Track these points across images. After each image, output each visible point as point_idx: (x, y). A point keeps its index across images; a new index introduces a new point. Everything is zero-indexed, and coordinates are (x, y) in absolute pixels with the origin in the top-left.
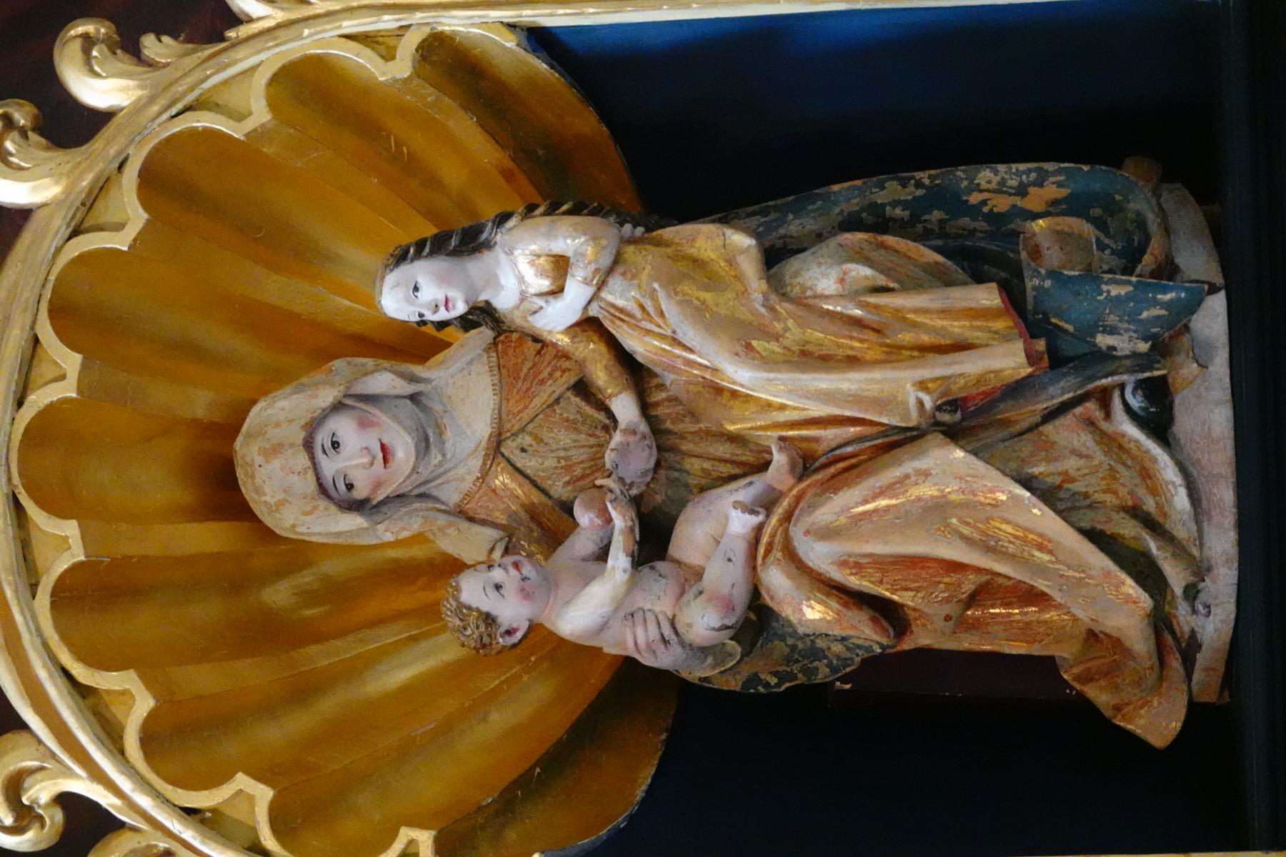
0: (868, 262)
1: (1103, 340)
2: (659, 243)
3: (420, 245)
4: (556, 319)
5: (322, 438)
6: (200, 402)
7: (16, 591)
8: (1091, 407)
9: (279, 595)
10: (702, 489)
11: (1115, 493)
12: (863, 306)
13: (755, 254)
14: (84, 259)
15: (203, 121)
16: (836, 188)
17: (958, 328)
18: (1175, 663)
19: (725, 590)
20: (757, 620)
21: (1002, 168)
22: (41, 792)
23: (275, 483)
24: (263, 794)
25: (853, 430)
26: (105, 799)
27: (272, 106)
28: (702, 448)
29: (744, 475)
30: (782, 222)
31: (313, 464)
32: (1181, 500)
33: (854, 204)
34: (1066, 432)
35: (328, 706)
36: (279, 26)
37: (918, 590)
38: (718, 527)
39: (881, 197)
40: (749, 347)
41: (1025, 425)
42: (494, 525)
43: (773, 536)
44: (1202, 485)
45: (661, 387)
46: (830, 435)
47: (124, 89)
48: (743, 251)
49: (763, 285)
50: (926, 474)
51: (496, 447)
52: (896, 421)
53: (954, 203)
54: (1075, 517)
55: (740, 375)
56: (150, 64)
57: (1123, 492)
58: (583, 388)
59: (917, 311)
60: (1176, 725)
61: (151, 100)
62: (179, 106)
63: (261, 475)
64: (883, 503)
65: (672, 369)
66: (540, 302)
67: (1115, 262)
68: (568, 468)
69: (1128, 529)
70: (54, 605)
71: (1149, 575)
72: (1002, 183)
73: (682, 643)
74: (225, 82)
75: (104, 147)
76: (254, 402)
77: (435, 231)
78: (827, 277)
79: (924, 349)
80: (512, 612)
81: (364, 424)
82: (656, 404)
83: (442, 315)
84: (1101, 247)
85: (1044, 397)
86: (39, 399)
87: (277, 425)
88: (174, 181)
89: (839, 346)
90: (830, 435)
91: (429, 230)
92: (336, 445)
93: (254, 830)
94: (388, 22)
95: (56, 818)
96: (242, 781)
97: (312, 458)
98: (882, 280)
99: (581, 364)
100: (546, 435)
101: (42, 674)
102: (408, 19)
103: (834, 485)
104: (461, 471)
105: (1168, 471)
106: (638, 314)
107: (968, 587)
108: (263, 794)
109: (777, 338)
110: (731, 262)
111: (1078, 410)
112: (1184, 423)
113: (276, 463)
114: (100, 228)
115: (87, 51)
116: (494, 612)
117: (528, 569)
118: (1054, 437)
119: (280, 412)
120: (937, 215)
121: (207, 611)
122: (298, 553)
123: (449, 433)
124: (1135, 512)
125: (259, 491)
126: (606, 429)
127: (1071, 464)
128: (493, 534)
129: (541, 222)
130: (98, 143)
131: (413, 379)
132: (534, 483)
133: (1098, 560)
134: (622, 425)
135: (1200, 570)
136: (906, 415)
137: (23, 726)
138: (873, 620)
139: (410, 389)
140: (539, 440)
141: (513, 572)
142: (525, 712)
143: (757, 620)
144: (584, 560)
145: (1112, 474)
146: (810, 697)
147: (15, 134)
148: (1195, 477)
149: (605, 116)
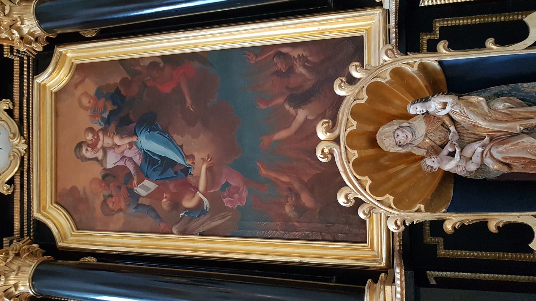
2: (463, 99)
4: (443, 113)
5: (396, 135)
6: (371, 128)
10: (468, 144)
13: (485, 101)
14: (357, 104)
17: (528, 115)
20: (482, 166)
21: (529, 83)
22: (351, 197)
24: (392, 198)
25: (503, 133)
26: (363, 198)
27: (391, 77)
29: (475, 141)
33: (496, 91)
36: (392, 62)
46: (498, 134)
47: (363, 75)
50: (524, 142)
51: (426, 136)
53: (519, 90)
58: (443, 125)
61: (368, 76)
64: (513, 147)
70: (353, 165)
72: (529, 86)
76: (379, 128)
78: (500, 105)
79: (520, 118)
80: (436, 166)
81: (403, 132)
86: (349, 130)
90: (498, 134)
96: (388, 195)
98: (512, 106)
100: (435, 133)
108: (392, 198)
109: (490, 117)
117: (438, 158)
120: (514, 92)
123: (416, 133)
130: (358, 84)
136: (517, 131)
137: (347, 185)
139: (409, 125)
143: (482, 166)
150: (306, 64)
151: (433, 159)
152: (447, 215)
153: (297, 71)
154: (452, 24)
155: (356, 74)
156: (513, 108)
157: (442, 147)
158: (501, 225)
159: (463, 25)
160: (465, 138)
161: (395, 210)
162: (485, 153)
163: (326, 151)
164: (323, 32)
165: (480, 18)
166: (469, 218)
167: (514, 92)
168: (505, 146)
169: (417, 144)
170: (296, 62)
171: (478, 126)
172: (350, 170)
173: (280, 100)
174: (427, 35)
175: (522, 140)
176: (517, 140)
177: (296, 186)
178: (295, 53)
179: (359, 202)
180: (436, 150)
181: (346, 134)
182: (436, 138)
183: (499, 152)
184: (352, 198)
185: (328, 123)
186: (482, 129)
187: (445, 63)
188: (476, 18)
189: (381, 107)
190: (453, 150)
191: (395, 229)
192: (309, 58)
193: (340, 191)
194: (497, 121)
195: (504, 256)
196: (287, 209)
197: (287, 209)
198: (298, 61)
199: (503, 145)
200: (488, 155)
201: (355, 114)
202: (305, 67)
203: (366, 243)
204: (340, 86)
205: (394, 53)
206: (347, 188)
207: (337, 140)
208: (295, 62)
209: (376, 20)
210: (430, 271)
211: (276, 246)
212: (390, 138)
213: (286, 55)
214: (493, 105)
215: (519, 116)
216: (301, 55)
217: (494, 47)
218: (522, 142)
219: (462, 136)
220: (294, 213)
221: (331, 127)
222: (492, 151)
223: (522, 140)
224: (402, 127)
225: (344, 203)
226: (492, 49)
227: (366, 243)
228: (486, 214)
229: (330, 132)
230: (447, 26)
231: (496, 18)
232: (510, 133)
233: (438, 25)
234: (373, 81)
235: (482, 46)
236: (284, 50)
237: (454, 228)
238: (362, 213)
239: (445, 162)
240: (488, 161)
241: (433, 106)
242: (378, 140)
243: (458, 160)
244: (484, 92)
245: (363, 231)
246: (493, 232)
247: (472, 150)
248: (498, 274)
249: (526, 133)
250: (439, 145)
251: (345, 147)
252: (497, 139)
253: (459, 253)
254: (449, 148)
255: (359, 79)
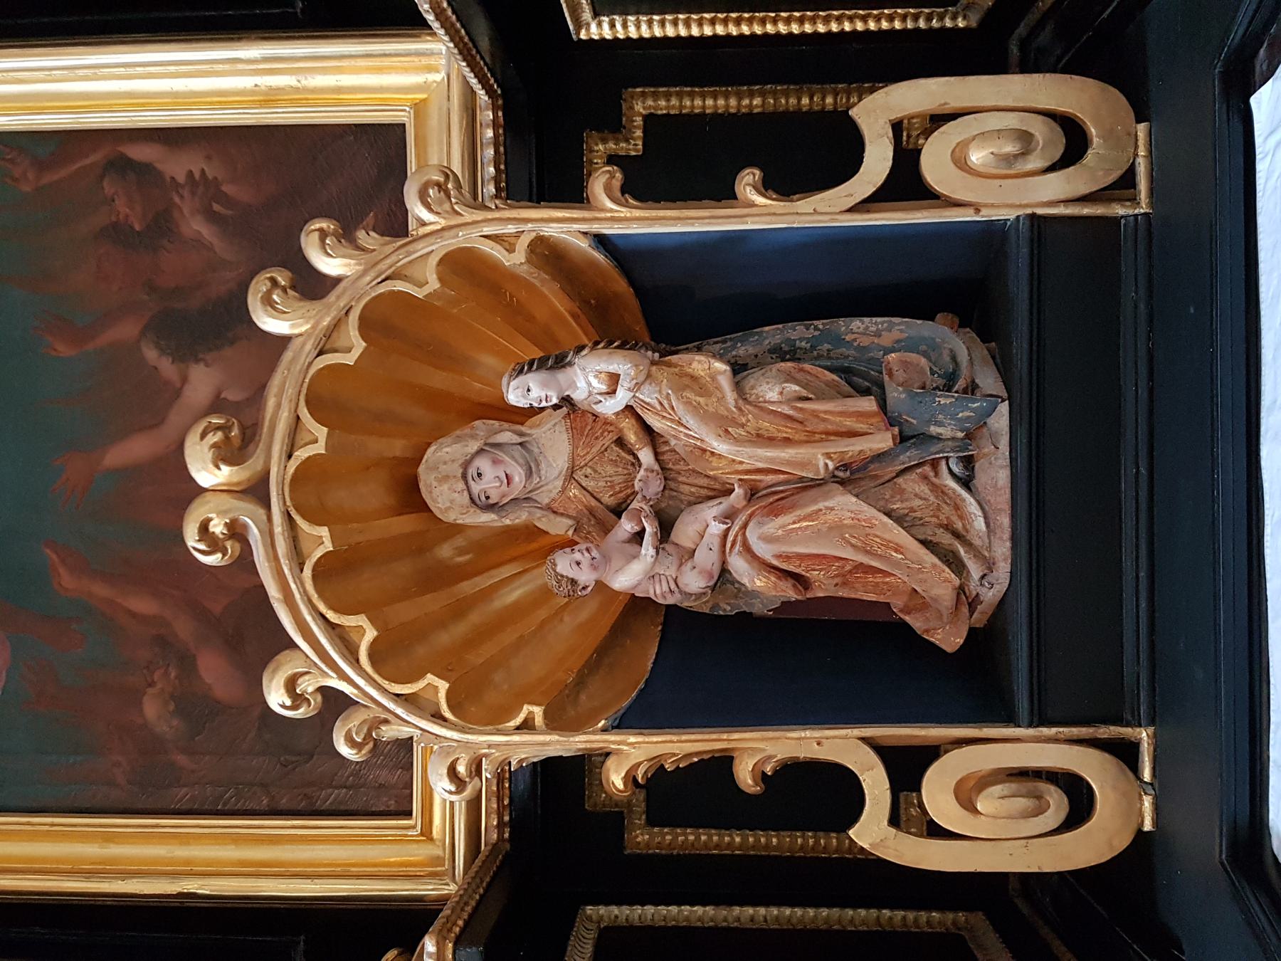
0: (797, 382)
1: (934, 430)
2: (669, 365)
3: (531, 364)
4: (610, 407)
5: (472, 471)
6: (398, 447)
7: (291, 570)
8: (927, 468)
9: (445, 551)
10: (691, 504)
11: (938, 517)
12: (796, 408)
13: (729, 373)
15: (399, 286)
16: (767, 328)
17: (850, 423)
18: (965, 610)
19: (709, 567)
21: (866, 320)
22: (307, 686)
23: (444, 497)
24: (443, 686)
27: (440, 279)
28: (691, 480)
29: (710, 498)
30: (734, 347)
31: (463, 481)
32: (980, 524)
33: (777, 339)
34: (911, 483)
35: (475, 617)
36: (443, 229)
37: (821, 570)
38: (703, 525)
39: (793, 335)
40: (726, 431)
41: (887, 478)
42: (569, 517)
43: (736, 536)
44: (992, 516)
45: (666, 443)
46: (770, 478)
47: (346, 265)
48: (720, 373)
49: (735, 395)
50: (832, 509)
52: (811, 476)
53: (838, 341)
54: (914, 531)
55: (721, 447)
56: (363, 249)
57: (942, 517)
58: (620, 442)
59: (825, 412)
60: (960, 641)
61: (365, 273)
62: (383, 277)
63: (436, 492)
65: (676, 437)
66: (600, 398)
67: (941, 382)
68: (612, 487)
69: (946, 539)
71: (956, 564)
72: (867, 328)
73: (681, 592)
74: (410, 262)
75: (336, 301)
76: (429, 445)
77: (542, 354)
78: (771, 389)
80: (586, 577)
81: (496, 462)
82: (663, 453)
83: (544, 404)
84: (933, 373)
85: (897, 462)
86: (302, 454)
87: (445, 463)
88: (387, 321)
89: (779, 431)
90: (770, 478)
91: (538, 354)
92: (479, 475)
93: (437, 704)
94: (511, 229)
95: (316, 701)
96: (430, 678)
97: (466, 483)
98: (804, 393)
99: (621, 430)
100: (599, 469)
101: (309, 618)
102: (522, 227)
103: (774, 511)
104: (550, 487)
105: (972, 506)
106: (659, 407)
107: (848, 568)
108: (443, 686)
109: (743, 426)
110: (713, 378)
111: (919, 471)
112: (982, 478)
113: (446, 487)
114: (336, 351)
115: (322, 240)
116: (576, 578)
117: (595, 553)
118: (904, 486)
119: (443, 457)
120: (827, 346)
121: (404, 568)
122: (455, 529)
123: (543, 466)
124: (948, 528)
125: (434, 501)
126: (633, 464)
127: (917, 503)
128: (570, 522)
129: (601, 351)
130: (332, 297)
131: (521, 434)
132: (592, 495)
133: (930, 558)
134: (644, 466)
135: (990, 565)
137: (296, 646)
138: (794, 586)
139: (520, 440)
140: (595, 471)
141: (586, 554)
142: (569, 637)
144: (624, 542)
145: (939, 508)
146: (745, 618)
147: (278, 291)
148: (987, 513)
149: (631, 282)
150: (216, 207)
151: (577, 556)
152: (612, 740)
153: (185, 230)
154: (681, 107)
155: (329, 265)
156: (808, 399)
157: (618, 511)
158: (768, 769)
159: (715, 116)
160: (685, 489)
161: (452, 726)
162: (730, 538)
163: (218, 527)
164: (270, 98)
165: (763, 94)
166: (679, 746)
167: (827, 346)
168: (781, 520)
169: (546, 501)
170: (182, 197)
171: (712, 453)
172: (305, 593)
173: (127, 330)
174: (604, 141)
175: (827, 504)
176: (815, 501)
177: (184, 628)
178: (177, 166)
179: (335, 703)
180: (600, 519)
181: (291, 469)
182: (602, 484)
183: (771, 537)
184: (310, 689)
185: (224, 428)
186: (724, 462)
187: (619, 243)
188: (751, 95)
189: (422, 371)
190: (637, 528)
191: (451, 793)
192: (224, 188)
193: (271, 667)
194: (762, 439)
195: (817, 842)
196: (152, 709)
197: (152, 709)
198: (186, 193)
199: (776, 516)
200: (737, 547)
201: (324, 399)
202: (212, 217)
203: (408, 814)
204: (268, 301)
205: (449, 197)
206: (296, 654)
207: (257, 491)
208: (177, 199)
209: (439, 77)
210: (595, 903)
211: (109, 838)
212: (463, 481)
213: (145, 172)
214: (753, 388)
215: (822, 427)
216: (197, 176)
217: (760, 200)
218: (827, 508)
219: (674, 480)
220: (175, 722)
221: (237, 443)
222: (748, 534)
223: (827, 504)
224: (498, 446)
225: (283, 706)
226: (753, 205)
227: (408, 814)
228: (725, 736)
229: (230, 463)
230: (668, 115)
231: (811, 98)
232: (802, 479)
233: (639, 107)
234: (382, 289)
235: (725, 194)
236: (139, 153)
237: (630, 778)
238: (342, 740)
239: (616, 563)
240: (739, 566)
241: (581, 384)
242: (421, 485)
243: (650, 560)
244: (741, 342)
245: (396, 777)
246: (742, 786)
247: (698, 527)
248: (792, 905)
249: (842, 482)
250: (607, 507)
251: (289, 515)
252: (770, 495)
253: (691, 838)
254: (627, 526)
255: (337, 281)
